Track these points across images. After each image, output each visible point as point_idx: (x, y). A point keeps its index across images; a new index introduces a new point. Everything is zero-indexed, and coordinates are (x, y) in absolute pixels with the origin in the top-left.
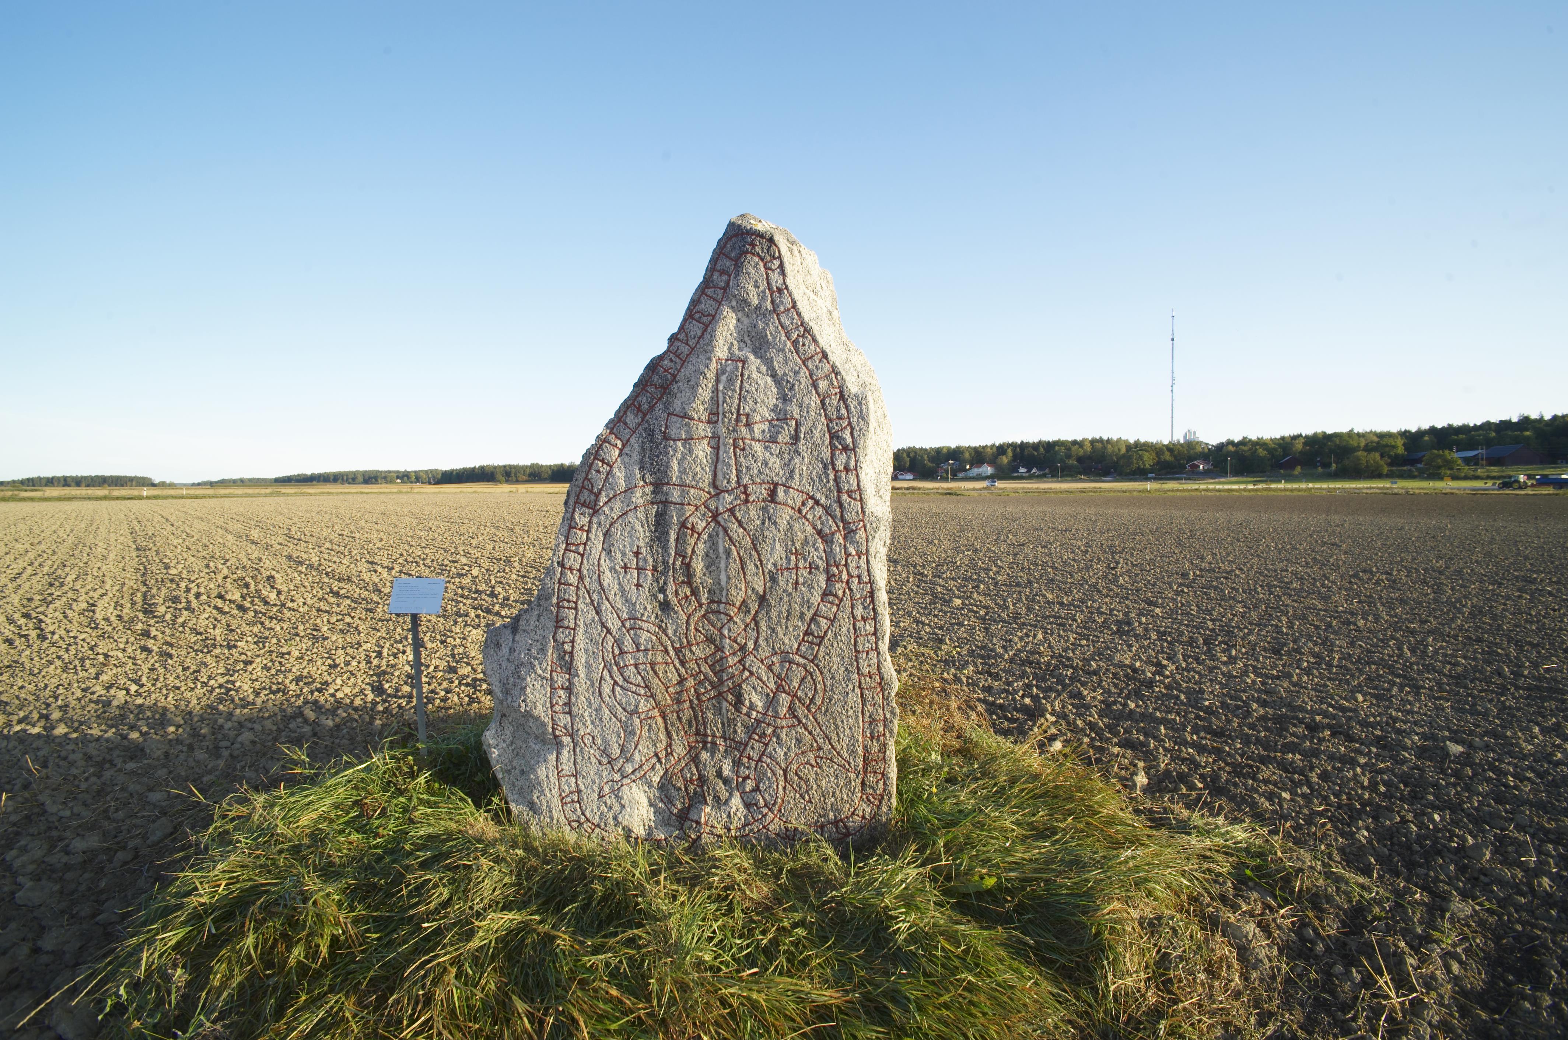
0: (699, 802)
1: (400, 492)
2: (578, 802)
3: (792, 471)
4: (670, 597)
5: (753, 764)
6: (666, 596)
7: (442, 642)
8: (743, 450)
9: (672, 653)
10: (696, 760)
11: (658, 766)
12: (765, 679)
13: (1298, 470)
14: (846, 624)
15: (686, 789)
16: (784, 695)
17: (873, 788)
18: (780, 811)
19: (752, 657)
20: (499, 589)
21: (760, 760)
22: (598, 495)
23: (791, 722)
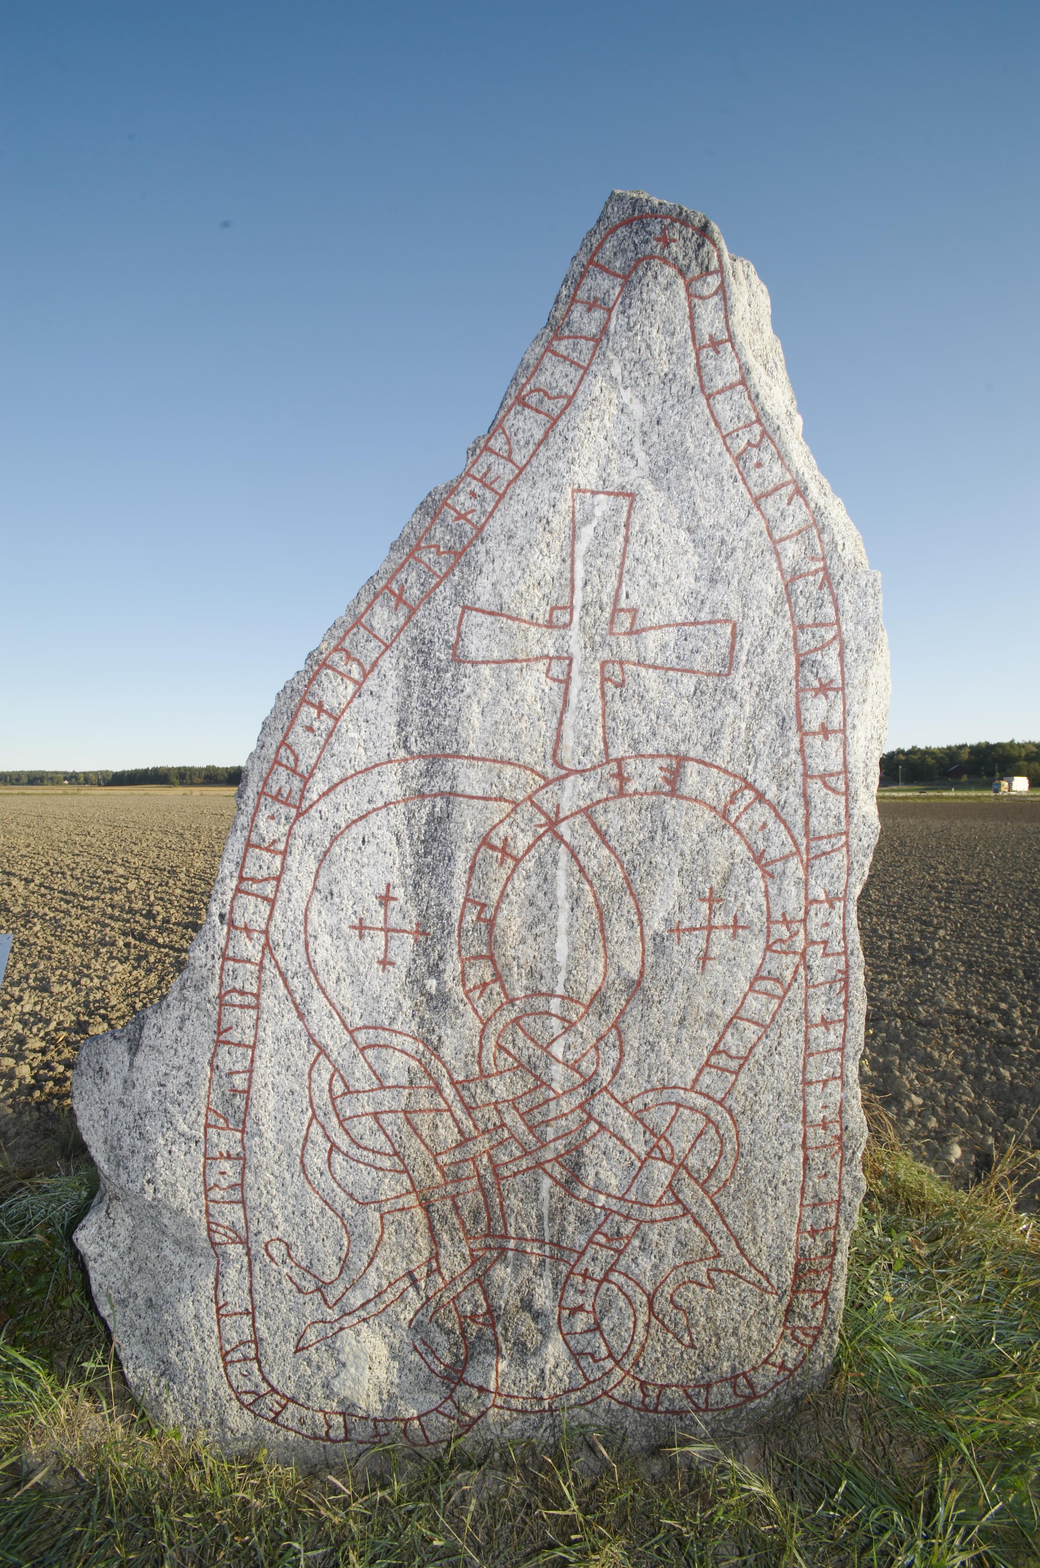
0: (487, 1351)
1: (66, 794)
2: (257, 1359)
3: (715, 733)
4: (450, 984)
5: (592, 1286)
6: (441, 983)
7: (75, 984)
8: (620, 685)
9: (449, 1091)
10: (482, 1280)
11: (411, 1292)
12: (627, 1136)
13: (965, 778)
14: (793, 1039)
15: (463, 1331)
16: (661, 1164)
17: (805, 1318)
18: (636, 1363)
19: (606, 1098)
20: (159, 908)
21: (606, 1279)
22: (305, 779)
23: (669, 1211)
